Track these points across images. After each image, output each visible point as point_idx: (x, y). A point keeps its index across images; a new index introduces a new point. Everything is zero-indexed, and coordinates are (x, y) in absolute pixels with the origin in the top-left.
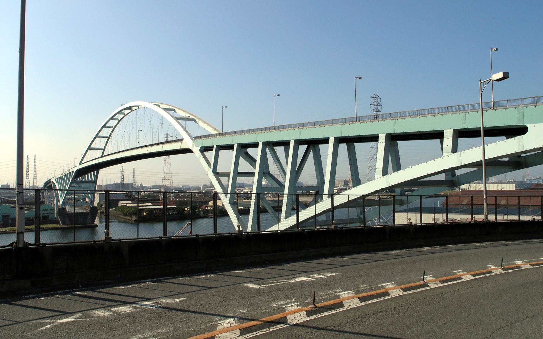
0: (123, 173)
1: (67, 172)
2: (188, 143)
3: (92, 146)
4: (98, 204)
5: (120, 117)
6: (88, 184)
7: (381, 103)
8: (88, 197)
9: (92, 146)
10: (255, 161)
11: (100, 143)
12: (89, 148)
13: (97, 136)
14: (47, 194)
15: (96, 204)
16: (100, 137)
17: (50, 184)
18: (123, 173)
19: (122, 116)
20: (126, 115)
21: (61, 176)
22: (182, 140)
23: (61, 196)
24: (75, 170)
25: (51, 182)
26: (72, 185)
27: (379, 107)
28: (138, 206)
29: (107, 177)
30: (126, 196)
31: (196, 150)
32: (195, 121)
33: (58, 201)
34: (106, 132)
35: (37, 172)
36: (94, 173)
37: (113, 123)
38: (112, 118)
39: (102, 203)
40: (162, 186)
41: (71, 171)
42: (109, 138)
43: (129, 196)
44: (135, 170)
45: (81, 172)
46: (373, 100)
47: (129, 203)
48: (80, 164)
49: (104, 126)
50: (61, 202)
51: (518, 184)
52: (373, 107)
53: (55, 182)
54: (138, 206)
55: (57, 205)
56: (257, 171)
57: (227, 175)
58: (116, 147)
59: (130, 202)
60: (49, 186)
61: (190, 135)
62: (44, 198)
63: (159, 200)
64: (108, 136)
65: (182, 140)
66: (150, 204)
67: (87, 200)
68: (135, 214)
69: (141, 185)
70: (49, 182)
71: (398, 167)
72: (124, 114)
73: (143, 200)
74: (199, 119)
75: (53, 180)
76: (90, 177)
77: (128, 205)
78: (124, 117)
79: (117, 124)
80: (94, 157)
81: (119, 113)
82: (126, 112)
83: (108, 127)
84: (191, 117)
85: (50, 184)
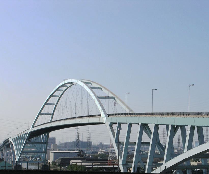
0: (78, 133)
1: (22, 134)
2: (104, 118)
3: (42, 112)
5: (64, 89)
6: (40, 145)
9: (42, 112)
10: (151, 133)
11: (49, 109)
12: (40, 114)
13: (46, 104)
16: (48, 104)
17: (8, 143)
18: (78, 133)
19: (65, 88)
20: (68, 88)
21: (17, 136)
23: (17, 154)
24: (28, 132)
25: (9, 141)
26: (26, 145)
29: (60, 137)
30: (78, 155)
34: (54, 100)
36: (45, 135)
37: (59, 93)
38: (57, 90)
39: (56, 161)
41: (25, 132)
43: (81, 156)
44: (90, 129)
45: (34, 134)
47: (79, 162)
48: (33, 127)
49: (52, 96)
50: (17, 160)
54: (82, 163)
55: (14, 161)
58: (62, 114)
59: (80, 161)
63: (107, 160)
64: (55, 103)
66: (99, 163)
72: (62, 91)
73: (94, 159)
74: (117, 97)
75: (11, 140)
76: (42, 138)
77: (78, 164)
78: (67, 89)
79: (71, 86)
80: (44, 122)
82: (68, 85)
84: (111, 95)
85: (8, 143)
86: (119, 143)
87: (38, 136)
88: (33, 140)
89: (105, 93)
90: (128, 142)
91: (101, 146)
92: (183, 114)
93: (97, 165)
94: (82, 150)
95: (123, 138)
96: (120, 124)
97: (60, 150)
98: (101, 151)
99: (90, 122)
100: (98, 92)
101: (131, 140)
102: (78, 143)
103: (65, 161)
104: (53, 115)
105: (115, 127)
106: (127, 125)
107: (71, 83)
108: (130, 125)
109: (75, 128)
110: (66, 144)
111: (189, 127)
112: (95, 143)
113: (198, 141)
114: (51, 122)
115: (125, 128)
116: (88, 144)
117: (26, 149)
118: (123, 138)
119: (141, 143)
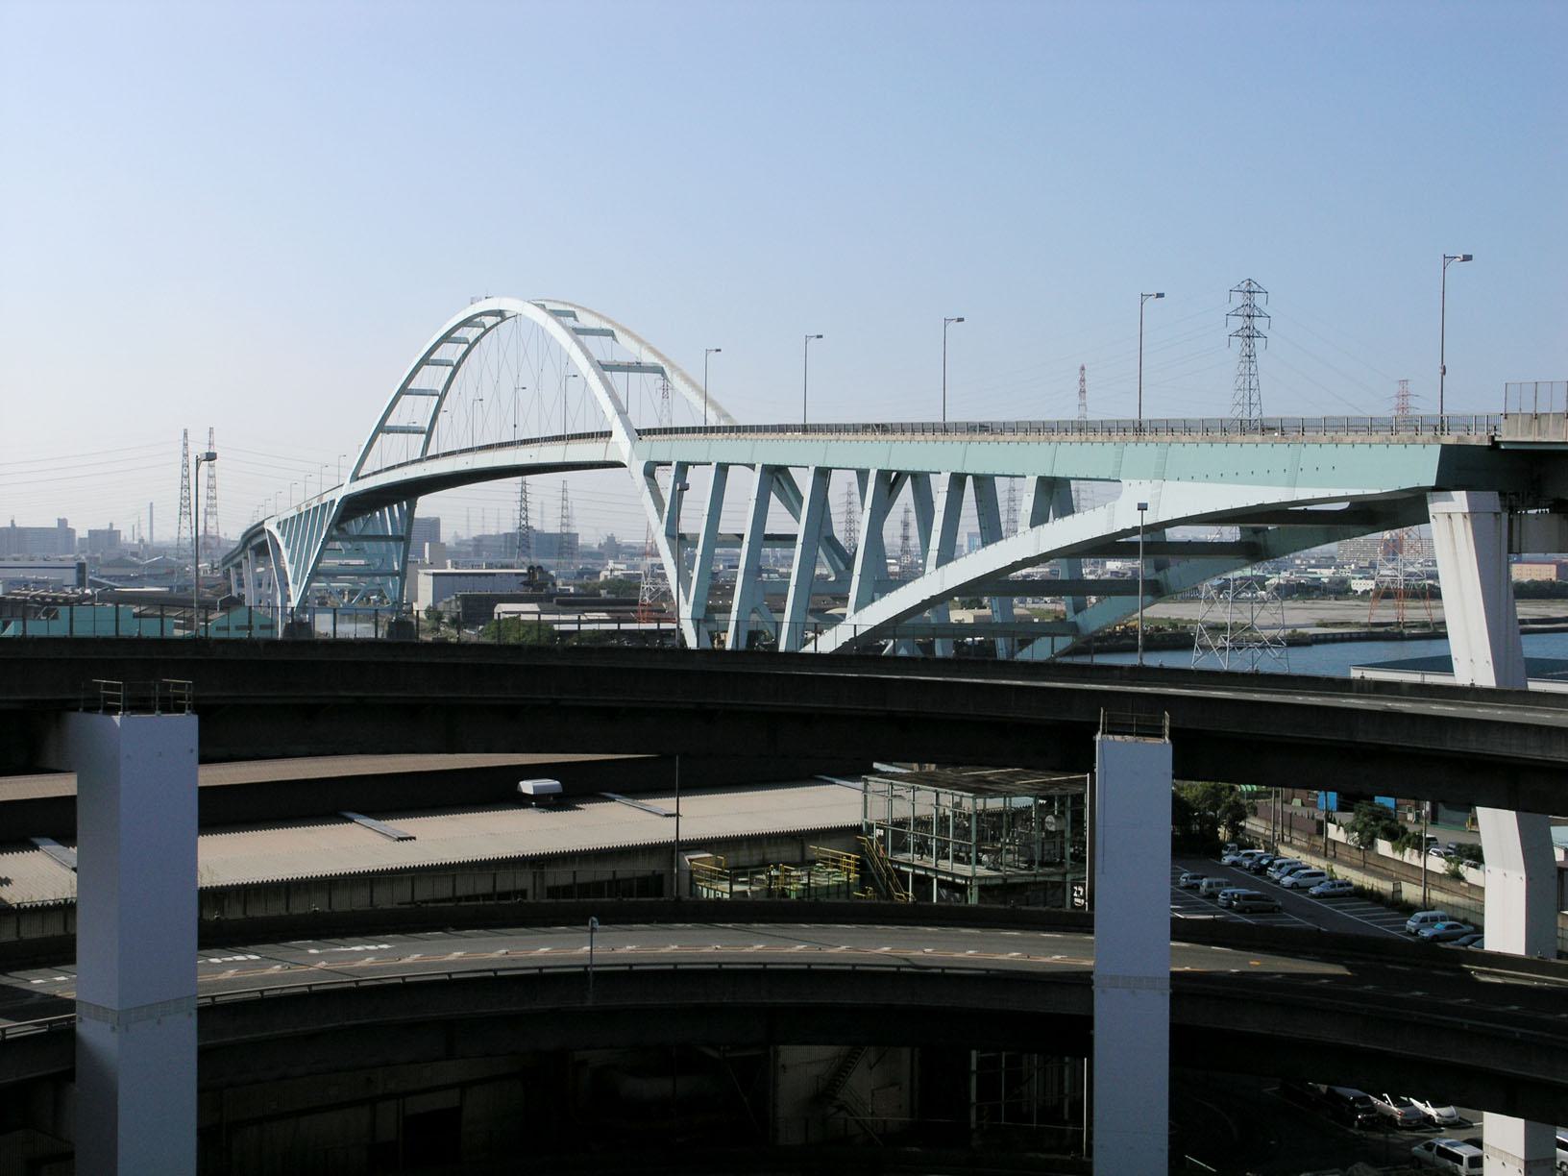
0: (524, 500)
1: (315, 503)
2: (621, 446)
3: (389, 423)
5: (471, 333)
7: (1266, 310)
9: (389, 423)
10: (800, 499)
11: (415, 411)
12: (382, 428)
13: (404, 390)
14: (253, 570)
16: (411, 393)
17: (259, 540)
18: (524, 500)
21: (294, 512)
22: (609, 434)
23: (295, 582)
24: (338, 496)
25: (263, 531)
26: (331, 545)
27: (1259, 324)
28: (539, 614)
29: (458, 517)
30: (524, 584)
31: (637, 468)
34: (432, 378)
35: (219, 492)
36: (400, 508)
37: (451, 352)
38: (446, 338)
39: (441, 607)
41: (326, 499)
42: (442, 398)
43: (536, 587)
44: (569, 486)
45: (359, 505)
46: (1239, 299)
47: (528, 611)
48: (355, 477)
49: (425, 361)
50: (294, 603)
52: (1238, 323)
53: (277, 534)
54: (539, 614)
55: (284, 607)
56: (800, 530)
58: (465, 430)
59: (534, 607)
60: (257, 543)
61: (627, 424)
62: (241, 585)
65: (609, 434)
66: (604, 616)
69: (611, 539)
70: (257, 531)
72: (466, 341)
73: (584, 600)
74: (672, 366)
75: (271, 526)
76: (388, 518)
77: (524, 617)
78: (483, 335)
80: (396, 460)
82: (489, 321)
83: (436, 363)
84: (649, 359)
85: (259, 540)
86: (679, 540)
87: (374, 510)
88: (355, 526)
89: (628, 349)
91: (613, 548)
92: (923, 428)
93: (596, 622)
94: (538, 563)
95: (694, 522)
96: (683, 468)
97: (455, 565)
98: (613, 569)
101: (725, 527)
102: (525, 539)
103: (477, 608)
104: (429, 434)
105: (666, 478)
106: (711, 471)
107: (500, 313)
109: (515, 481)
110: (479, 543)
112: (589, 537)
114: (425, 458)
115: (701, 481)
116: (564, 544)
117: (329, 563)
118: (694, 522)
119: (763, 539)
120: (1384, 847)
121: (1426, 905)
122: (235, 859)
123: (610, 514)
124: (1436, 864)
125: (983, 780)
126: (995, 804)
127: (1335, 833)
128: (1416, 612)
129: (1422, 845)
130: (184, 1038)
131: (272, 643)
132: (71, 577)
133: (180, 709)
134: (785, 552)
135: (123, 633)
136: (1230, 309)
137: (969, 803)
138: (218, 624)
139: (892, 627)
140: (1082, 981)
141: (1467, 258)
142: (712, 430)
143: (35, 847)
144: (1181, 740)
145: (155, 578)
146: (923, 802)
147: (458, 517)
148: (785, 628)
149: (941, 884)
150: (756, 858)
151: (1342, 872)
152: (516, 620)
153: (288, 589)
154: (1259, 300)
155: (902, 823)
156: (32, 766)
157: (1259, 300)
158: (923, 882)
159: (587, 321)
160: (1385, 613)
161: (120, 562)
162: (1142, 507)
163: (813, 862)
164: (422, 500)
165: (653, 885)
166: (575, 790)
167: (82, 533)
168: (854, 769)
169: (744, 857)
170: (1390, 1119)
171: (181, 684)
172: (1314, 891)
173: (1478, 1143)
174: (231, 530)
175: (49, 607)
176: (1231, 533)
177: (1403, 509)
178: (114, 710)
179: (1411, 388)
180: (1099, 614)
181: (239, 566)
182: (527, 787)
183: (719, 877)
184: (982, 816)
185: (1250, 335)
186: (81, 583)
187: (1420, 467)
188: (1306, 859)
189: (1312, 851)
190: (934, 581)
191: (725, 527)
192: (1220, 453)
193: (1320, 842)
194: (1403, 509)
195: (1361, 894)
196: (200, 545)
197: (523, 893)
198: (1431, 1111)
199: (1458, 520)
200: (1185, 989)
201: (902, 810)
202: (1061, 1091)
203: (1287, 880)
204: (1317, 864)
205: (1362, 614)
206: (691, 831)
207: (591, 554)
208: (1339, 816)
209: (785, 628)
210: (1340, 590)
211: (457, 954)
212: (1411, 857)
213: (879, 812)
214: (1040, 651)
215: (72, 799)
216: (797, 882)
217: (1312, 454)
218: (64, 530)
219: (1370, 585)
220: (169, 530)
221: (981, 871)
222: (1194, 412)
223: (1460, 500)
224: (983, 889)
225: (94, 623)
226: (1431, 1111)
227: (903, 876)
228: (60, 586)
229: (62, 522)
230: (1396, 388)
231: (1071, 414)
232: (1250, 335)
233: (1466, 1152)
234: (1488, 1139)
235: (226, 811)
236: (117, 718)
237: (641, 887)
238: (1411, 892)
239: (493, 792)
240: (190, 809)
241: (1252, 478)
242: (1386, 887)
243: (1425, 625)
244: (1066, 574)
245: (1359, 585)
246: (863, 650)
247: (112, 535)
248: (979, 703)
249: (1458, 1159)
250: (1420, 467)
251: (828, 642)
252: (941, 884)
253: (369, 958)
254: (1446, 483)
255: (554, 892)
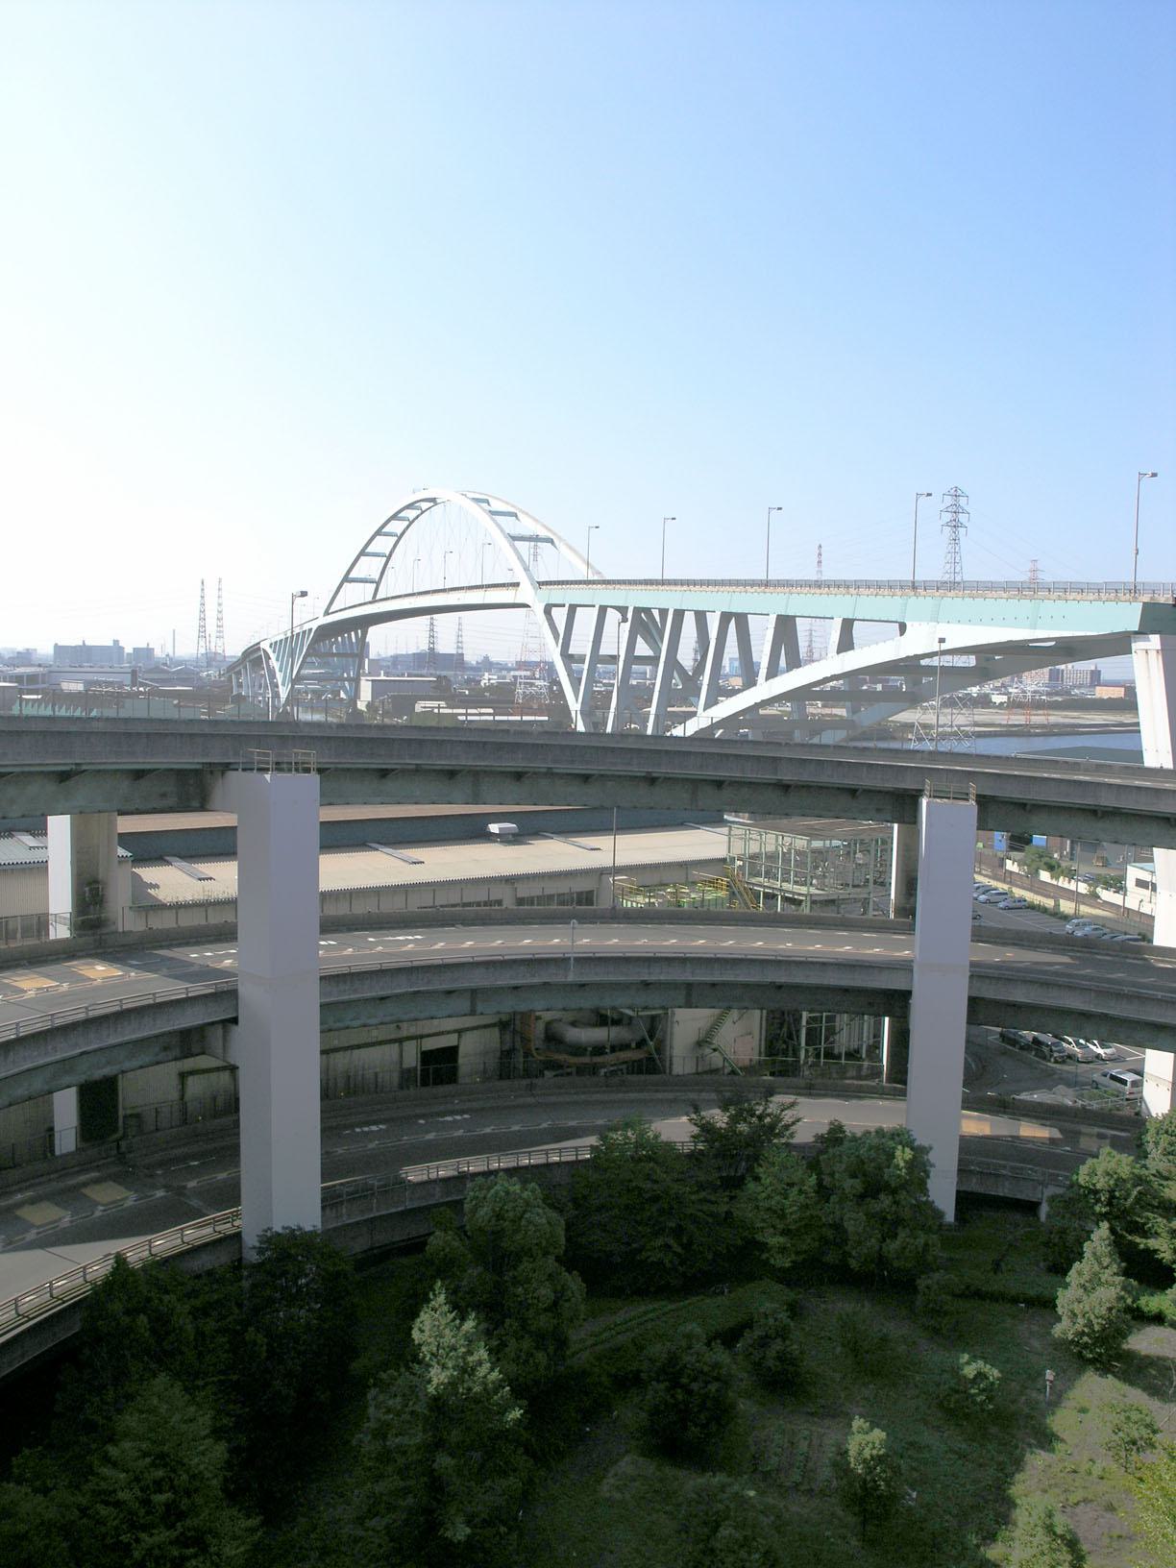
2: (526, 593)
4: (369, 706)
5: (411, 514)
8: (343, 688)
11: (369, 567)
12: (346, 579)
13: (363, 553)
15: (361, 706)
24: (314, 626)
27: (962, 518)
29: (383, 641)
31: (539, 609)
32: (552, 542)
33: (276, 695)
37: (396, 527)
40: (537, 664)
41: (306, 627)
42: (389, 558)
43: (442, 689)
45: (326, 632)
48: (327, 613)
49: (378, 533)
51: (88, 683)
53: (270, 651)
57: (581, 659)
58: (401, 582)
59: (443, 704)
60: (253, 657)
61: (531, 578)
65: (517, 585)
67: (343, 695)
68: (1129, 1357)
71: (795, 663)
73: (477, 699)
75: (265, 645)
80: (354, 600)
81: (410, 506)
82: (425, 505)
84: (543, 533)
86: (568, 658)
87: (338, 640)
88: (322, 647)
89: (527, 527)
90: (596, 657)
91: (487, 665)
92: (753, 583)
93: (483, 715)
94: (441, 671)
95: (581, 645)
96: (573, 608)
97: (387, 674)
98: (487, 679)
99: (487, 601)
100: (507, 523)
101: (606, 649)
102: (430, 658)
103: (405, 703)
104: (378, 584)
105: (560, 616)
106: (595, 611)
107: (433, 500)
108: (603, 610)
109: (425, 619)
110: (396, 660)
111: (718, 614)
112: (471, 657)
113: (737, 655)
114: (374, 601)
115: (586, 620)
116: (457, 661)
117: (305, 672)
118: (581, 645)
119: (632, 659)
120: (1045, 876)
121: (1076, 916)
122: (346, 871)
123: (501, 641)
124: (1083, 888)
125: (811, 827)
126: (817, 844)
127: (1010, 866)
128: (1127, 719)
129: (1071, 875)
130: (311, 998)
131: (267, 723)
132: (128, 679)
133: (307, 770)
134: (611, 667)
135: (154, 715)
136: (943, 507)
137: (801, 843)
138: (226, 711)
139: (723, 723)
140: (906, 967)
141: (1154, 475)
142: (593, 582)
143: (169, 863)
144: (983, 801)
145: (183, 681)
146: (769, 841)
147: (383, 641)
148: (652, 718)
149: (785, 899)
150: (656, 881)
151: (1018, 892)
152: (429, 714)
153: (281, 688)
154: (962, 501)
155: (755, 857)
156: (203, 807)
157: (962, 501)
158: (770, 897)
159: (496, 506)
160: (1018, 719)
161: (157, 669)
162: (942, 641)
163: (694, 883)
164: (372, 630)
165: (587, 898)
166: (528, 830)
167: (129, 650)
168: (715, 820)
169: (654, 879)
170: (1098, 1056)
171: (313, 758)
172: (1001, 905)
173: (1140, 1073)
174: (234, 649)
175: (119, 698)
176: (971, 661)
177: (1118, 644)
178: (266, 770)
179: (1039, 566)
180: (868, 716)
181: (239, 673)
182: (494, 828)
183: (638, 892)
184: (815, 851)
185: (956, 525)
186: (134, 684)
187: (1126, 617)
188: (994, 883)
189: (995, 878)
190: (765, 689)
191: (606, 649)
192: (1025, 606)
193: (1001, 873)
194: (1118, 644)
195: (1032, 907)
196: (211, 659)
197: (499, 902)
198: (1100, 1051)
199: (1153, 655)
200: (979, 973)
201: (754, 848)
202: (861, 1038)
203: (983, 897)
204: (1002, 887)
205: (1002, 718)
206: (624, 859)
207: (473, 669)
208: (1013, 854)
209: (652, 718)
210: (984, 701)
211: (644, 941)
212: (1063, 882)
213: (738, 849)
214: (828, 738)
215: (234, 829)
216: (690, 896)
217: (1050, 607)
218: (117, 647)
219: (1004, 699)
220: (187, 649)
221: (813, 890)
222: (1097, 577)
223: (1155, 641)
224: (814, 902)
225: (161, 710)
226: (1100, 1051)
227: (757, 895)
228: (121, 685)
229: (116, 642)
230: (1030, 566)
231: (811, 575)
232: (956, 525)
233: (1129, 1077)
234: (1148, 1069)
235: (341, 838)
236: (268, 777)
237: (579, 899)
238: (1067, 907)
239: (472, 831)
240: (242, 841)
241: (1004, 622)
242: (1049, 903)
243: (1043, 726)
244: (853, 687)
245: (997, 699)
246: (703, 737)
247: (148, 652)
248: (826, 774)
249: (1124, 1082)
250: (1126, 617)
251: (691, 727)
252: (785, 899)
253: (409, 945)
254: (1143, 632)
255: (520, 901)
